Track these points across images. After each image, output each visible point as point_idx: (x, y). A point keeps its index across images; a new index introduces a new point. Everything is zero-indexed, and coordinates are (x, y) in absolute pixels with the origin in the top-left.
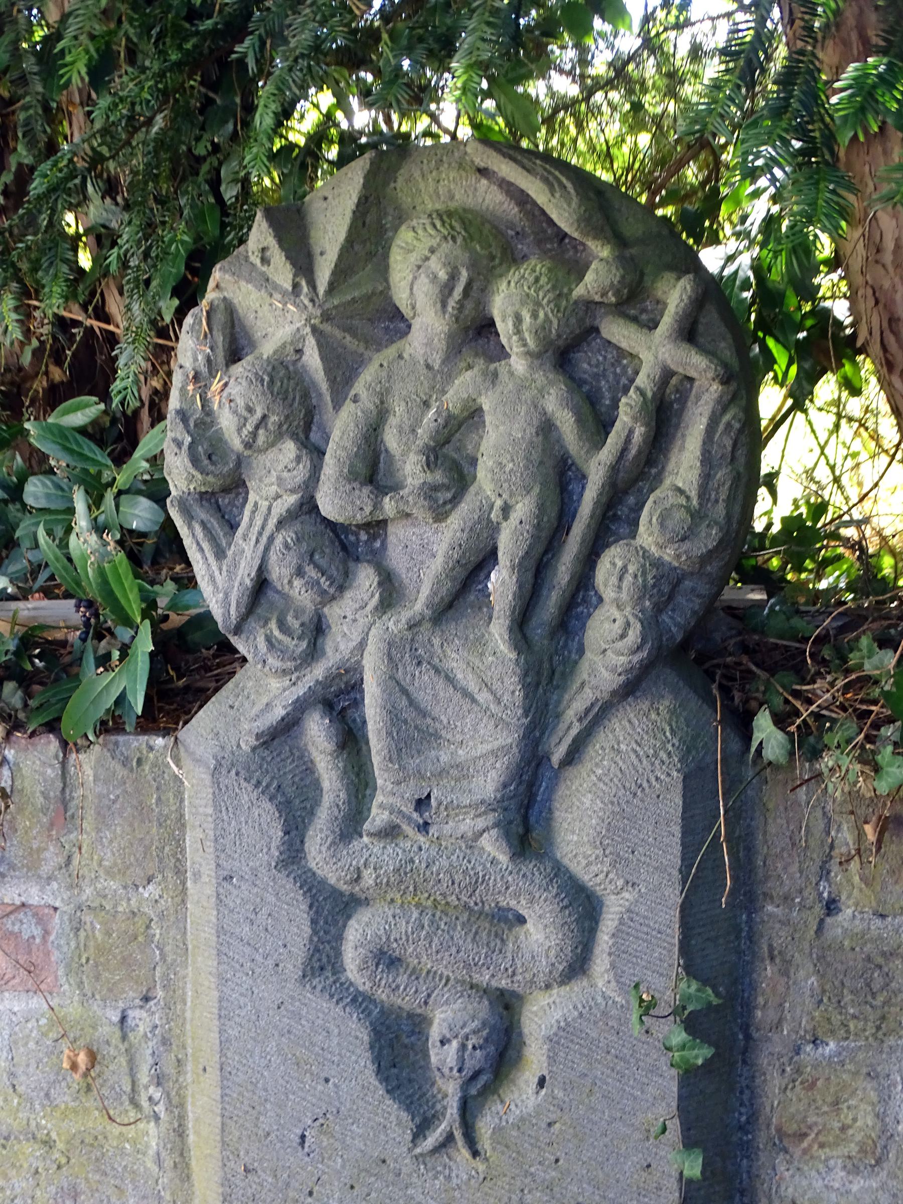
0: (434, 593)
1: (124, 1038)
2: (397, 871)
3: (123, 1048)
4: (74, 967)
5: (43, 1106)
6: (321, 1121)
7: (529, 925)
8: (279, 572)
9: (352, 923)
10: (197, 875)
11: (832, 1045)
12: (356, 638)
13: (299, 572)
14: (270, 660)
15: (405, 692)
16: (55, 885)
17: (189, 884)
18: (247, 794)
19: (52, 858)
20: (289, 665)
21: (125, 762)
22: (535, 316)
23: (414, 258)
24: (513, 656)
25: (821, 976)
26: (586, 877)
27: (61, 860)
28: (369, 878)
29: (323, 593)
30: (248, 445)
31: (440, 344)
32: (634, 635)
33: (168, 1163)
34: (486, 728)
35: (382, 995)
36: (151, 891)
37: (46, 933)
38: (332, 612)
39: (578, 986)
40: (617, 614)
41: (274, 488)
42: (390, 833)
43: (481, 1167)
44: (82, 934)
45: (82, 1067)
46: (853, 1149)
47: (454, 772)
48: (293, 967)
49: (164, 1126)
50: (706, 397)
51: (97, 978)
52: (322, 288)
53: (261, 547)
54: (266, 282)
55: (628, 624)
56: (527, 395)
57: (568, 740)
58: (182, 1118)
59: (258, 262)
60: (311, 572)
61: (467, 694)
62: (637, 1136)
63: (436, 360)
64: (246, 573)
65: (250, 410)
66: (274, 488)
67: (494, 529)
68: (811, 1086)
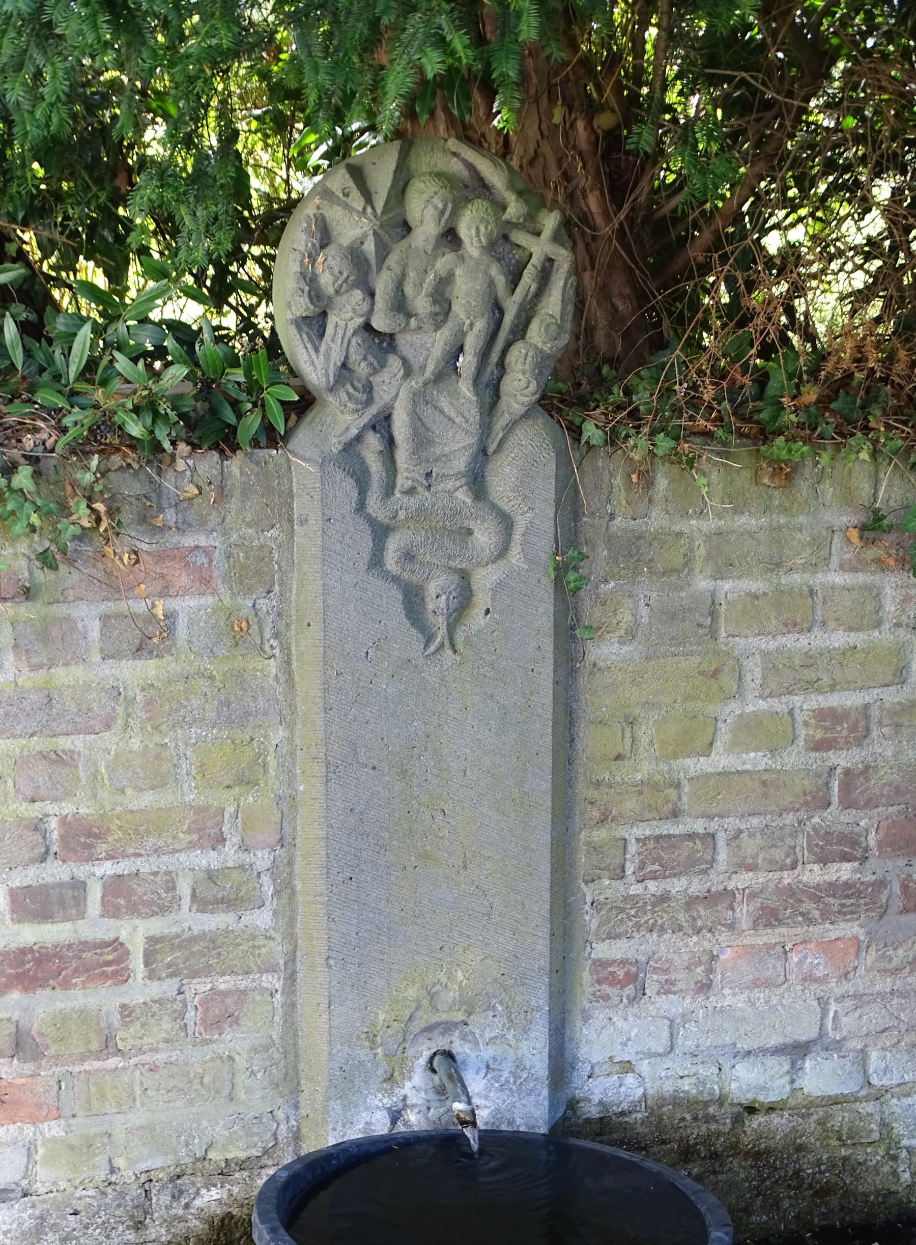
0: (436, 367)
1: (256, 615)
2: (417, 510)
3: (256, 620)
4: (227, 579)
5: (209, 657)
6: (377, 645)
7: (477, 534)
8: (355, 357)
9: (389, 539)
10: (304, 522)
11: (612, 584)
12: (393, 393)
13: (365, 359)
14: (349, 404)
15: (420, 419)
16: (215, 534)
17: (296, 527)
18: (339, 475)
19: (214, 518)
20: (360, 406)
21: (258, 464)
22: (486, 228)
23: (425, 196)
24: (475, 398)
25: (609, 550)
26: (507, 508)
27: (220, 520)
28: (402, 515)
29: (375, 369)
30: (337, 292)
31: (432, 241)
32: (533, 386)
33: (282, 679)
34: (460, 435)
35: (406, 576)
36: (273, 532)
37: (211, 561)
38: (376, 380)
39: (502, 563)
40: (521, 376)
41: (351, 314)
42: (411, 491)
43: (458, 658)
44: (232, 560)
45: (245, 629)
46: (622, 632)
47: (443, 459)
48: (362, 566)
49: (279, 661)
50: (561, 270)
51: (241, 583)
52: (379, 212)
53: (345, 345)
54: (346, 206)
55: (529, 382)
56: (482, 267)
57: (498, 440)
58: (289, 655)
59: (341, 195)
60: (371, 359)
61: (450, 419)
62: (534, 633)
63: (429, 248)
64: (336, 358)
65: (341, 273)
66: (351, 314)
67: (464, 335)
68: (604, 604)
